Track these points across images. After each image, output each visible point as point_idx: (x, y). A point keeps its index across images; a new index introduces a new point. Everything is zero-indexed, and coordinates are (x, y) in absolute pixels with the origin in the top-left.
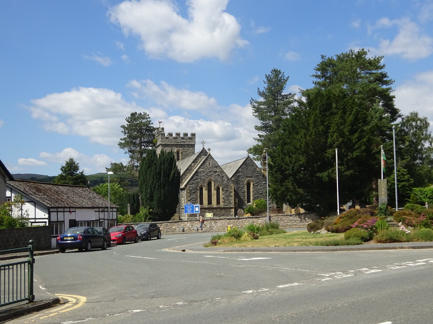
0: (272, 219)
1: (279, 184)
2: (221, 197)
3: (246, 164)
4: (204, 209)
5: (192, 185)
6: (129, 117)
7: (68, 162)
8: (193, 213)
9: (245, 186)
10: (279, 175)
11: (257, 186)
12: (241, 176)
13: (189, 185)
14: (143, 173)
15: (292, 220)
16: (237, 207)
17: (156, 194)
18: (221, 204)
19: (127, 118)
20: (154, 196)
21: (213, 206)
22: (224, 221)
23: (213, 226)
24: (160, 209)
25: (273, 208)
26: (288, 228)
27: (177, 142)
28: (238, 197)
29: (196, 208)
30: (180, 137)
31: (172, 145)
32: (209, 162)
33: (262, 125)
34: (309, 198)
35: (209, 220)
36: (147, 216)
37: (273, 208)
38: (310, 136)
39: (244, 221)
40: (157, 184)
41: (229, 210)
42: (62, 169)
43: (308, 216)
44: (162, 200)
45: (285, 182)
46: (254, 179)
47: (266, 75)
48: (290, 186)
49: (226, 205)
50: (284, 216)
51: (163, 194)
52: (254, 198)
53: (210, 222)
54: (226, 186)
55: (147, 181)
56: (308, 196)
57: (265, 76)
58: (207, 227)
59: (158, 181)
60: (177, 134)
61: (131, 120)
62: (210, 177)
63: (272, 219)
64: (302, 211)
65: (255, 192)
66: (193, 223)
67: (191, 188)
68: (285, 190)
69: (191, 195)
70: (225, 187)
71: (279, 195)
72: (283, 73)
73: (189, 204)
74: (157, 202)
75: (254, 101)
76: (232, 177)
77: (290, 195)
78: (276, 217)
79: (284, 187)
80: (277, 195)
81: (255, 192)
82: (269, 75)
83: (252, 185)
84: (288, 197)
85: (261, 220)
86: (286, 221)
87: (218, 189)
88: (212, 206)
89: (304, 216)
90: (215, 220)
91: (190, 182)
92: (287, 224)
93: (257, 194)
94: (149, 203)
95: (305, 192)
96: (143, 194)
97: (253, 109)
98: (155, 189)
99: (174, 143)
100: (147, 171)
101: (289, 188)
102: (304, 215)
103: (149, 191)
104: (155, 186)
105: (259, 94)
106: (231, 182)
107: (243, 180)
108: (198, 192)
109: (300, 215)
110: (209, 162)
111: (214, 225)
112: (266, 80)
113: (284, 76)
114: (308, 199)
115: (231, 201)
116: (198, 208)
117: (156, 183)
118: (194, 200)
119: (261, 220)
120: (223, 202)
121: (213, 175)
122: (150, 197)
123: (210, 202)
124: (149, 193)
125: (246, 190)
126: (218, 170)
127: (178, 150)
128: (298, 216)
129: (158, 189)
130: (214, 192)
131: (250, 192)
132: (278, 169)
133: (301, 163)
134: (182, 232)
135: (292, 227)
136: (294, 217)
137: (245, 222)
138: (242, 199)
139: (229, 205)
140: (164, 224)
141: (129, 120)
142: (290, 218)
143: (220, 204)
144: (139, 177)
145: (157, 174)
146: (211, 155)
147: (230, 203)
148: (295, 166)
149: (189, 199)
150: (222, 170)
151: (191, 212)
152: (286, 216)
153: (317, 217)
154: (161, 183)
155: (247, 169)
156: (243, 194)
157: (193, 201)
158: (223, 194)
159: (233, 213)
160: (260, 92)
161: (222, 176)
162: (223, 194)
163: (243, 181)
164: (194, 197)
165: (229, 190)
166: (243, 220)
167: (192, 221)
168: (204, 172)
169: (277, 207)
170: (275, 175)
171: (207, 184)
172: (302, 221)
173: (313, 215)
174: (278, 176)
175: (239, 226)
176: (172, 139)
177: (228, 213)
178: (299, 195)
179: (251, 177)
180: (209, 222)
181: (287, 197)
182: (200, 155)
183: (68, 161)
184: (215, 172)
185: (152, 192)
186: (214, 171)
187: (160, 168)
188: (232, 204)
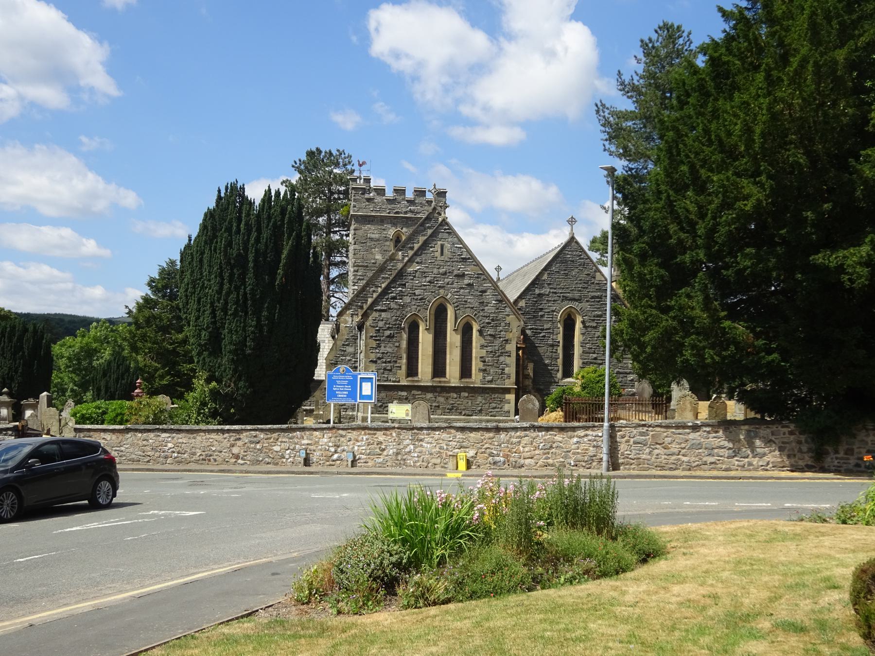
0: (623, 437)
1: (654, 304)
2: (474, 355)
4: (418, 391)
5: (384, 315)
6: (300, 161)
7: (164, 269)
8: (353, 402)
9: (559, 325)
10: (653, 270)
12: (548, 295)
14: (192, 258)
15: (699, 446)
16: (531, 387)
17: (230, 331)
18: (473, 375)
19: (296, 163)
20: (223, 336)
21: (449, 382)
22: (445, 435)
23: (407, 450)
24: (241, 384)
25: (641, 394)
26: (682, 477)
27: (397, 213)
28: (535, 358)
29: (364, 384)
30: (404, 199)
31: (382, 220)
32: (442, 246)
33: (624, 172)
34: (773, 361)
35: (394, 428)
36: (204, 404)
37: (641, 394)
38: (796, 80)
39: (515, 440)
40: (233, 296)
41: (500, 396)
42: (151, 283)
43: (764, 431)
44: (248, 351)
45: (675, 295)
46: (586, 306)
47: (642, 41)
48: (698, 312)
49: (491, 382)
50: (667, 427)
51: (253, 332)
52: (583, 363)
53: (399, 434)
54: (493, 320)
55: (203, 287)
56: (769, 352)
57: (640, 43)
58: (385, 453)
59: (237, 288)
60: (396, 191)
61: (306, 168)
62: (442, 291)
63: (623, 437)
64: (735, 410)
66: (342, 436)
67: (381, 324)
68: (675, 328)
69: (379, 346)
70: (490, 323)
71: (653, 347)
72: (690, 33)
73: (341, 370)
74: (231, 357)
75: (608, 109)
76: (520, 297)
77: (694, 347)
78: (635, 431)
79: (672, 314)
80: (642, 346)
82: (650, 40)
83: (578, 326)
84: (687, 353)
85: (580, 437)
86: (675, 447)
87: (466, 332)
88: (445, 382)
89: (749, 431)
90: (413, 429)
92: (679, 460)
93: (594, 353)
94: (207, 360)
95: (757, 336)
96: (191, 330)
97: (603, 129)
98: (226, 314)
99: (389, 213)
100: (202, 253)
101: (692, 319)
102: (746, 427)
103: (206, 319)
104: (226, 303)
105: (621, 90)
106: (508, 309)
107: (552, 308)
108: (401, 337)
109: (732, 428)
110: (442, 246)
111: (412, 447)
112: (642, 54)
113: (691, 43)
114: (769, 363)
115: (507, 369)
116: (369, 384)
117: (228, 294)
118: (390, 362)
119: (580, 437)
120: (480, 370)
122: (209, 340)
123: (439, 369)
124: (208, 327)
125: (560, 338)
126: (470, 270)
127: (399, 234)
128: (725, 430)
129: (235, 314)
130: (453, 339)
131: (573, 346)
132: (652, 245)
133: (745, 205)
134: (301, 468)
135: (698, 473)
136: (709, 432)
137: (519, 442)
138: (547, 365)
140: (247, 436)
141: (302, 167)
142: (692, 436)
143: (470, 376)
144: (182, 272)
145: (232, 261)
146: (447, 224)
147: (502, 374)
148: (718, 224)
149: (373, 357)
151: (348, 396)
152: (678, 427)
153: (803, 438)
154: (245, 294)
155: (567, 275)
157: (385, 362)
158: (482, 347)
159: (510, 407)
160: (622, 83)
162: (482, 347)
163: (553, 311)
164: (390, 350)
165: (502, 333)
166: (513, 434)
167: (339, 429)
168: (424, 274)
169: (655, 394)
170: (637, 268)
171: (433, 312)
172: (739, 450)
173: (786, 430)
174: (651, 272)
175: (498, 455)
176: (383, 204)
177: (494, 405)
178: (732, 348)
179: (579, 300)
180: (394, 434)
181: (682, 355)
182: (422, 228)
183: (165, 266)
184: (457, 276)
185: (218, 324)
186: (456, 272)
187: (246, 243)
188: (509, 377)
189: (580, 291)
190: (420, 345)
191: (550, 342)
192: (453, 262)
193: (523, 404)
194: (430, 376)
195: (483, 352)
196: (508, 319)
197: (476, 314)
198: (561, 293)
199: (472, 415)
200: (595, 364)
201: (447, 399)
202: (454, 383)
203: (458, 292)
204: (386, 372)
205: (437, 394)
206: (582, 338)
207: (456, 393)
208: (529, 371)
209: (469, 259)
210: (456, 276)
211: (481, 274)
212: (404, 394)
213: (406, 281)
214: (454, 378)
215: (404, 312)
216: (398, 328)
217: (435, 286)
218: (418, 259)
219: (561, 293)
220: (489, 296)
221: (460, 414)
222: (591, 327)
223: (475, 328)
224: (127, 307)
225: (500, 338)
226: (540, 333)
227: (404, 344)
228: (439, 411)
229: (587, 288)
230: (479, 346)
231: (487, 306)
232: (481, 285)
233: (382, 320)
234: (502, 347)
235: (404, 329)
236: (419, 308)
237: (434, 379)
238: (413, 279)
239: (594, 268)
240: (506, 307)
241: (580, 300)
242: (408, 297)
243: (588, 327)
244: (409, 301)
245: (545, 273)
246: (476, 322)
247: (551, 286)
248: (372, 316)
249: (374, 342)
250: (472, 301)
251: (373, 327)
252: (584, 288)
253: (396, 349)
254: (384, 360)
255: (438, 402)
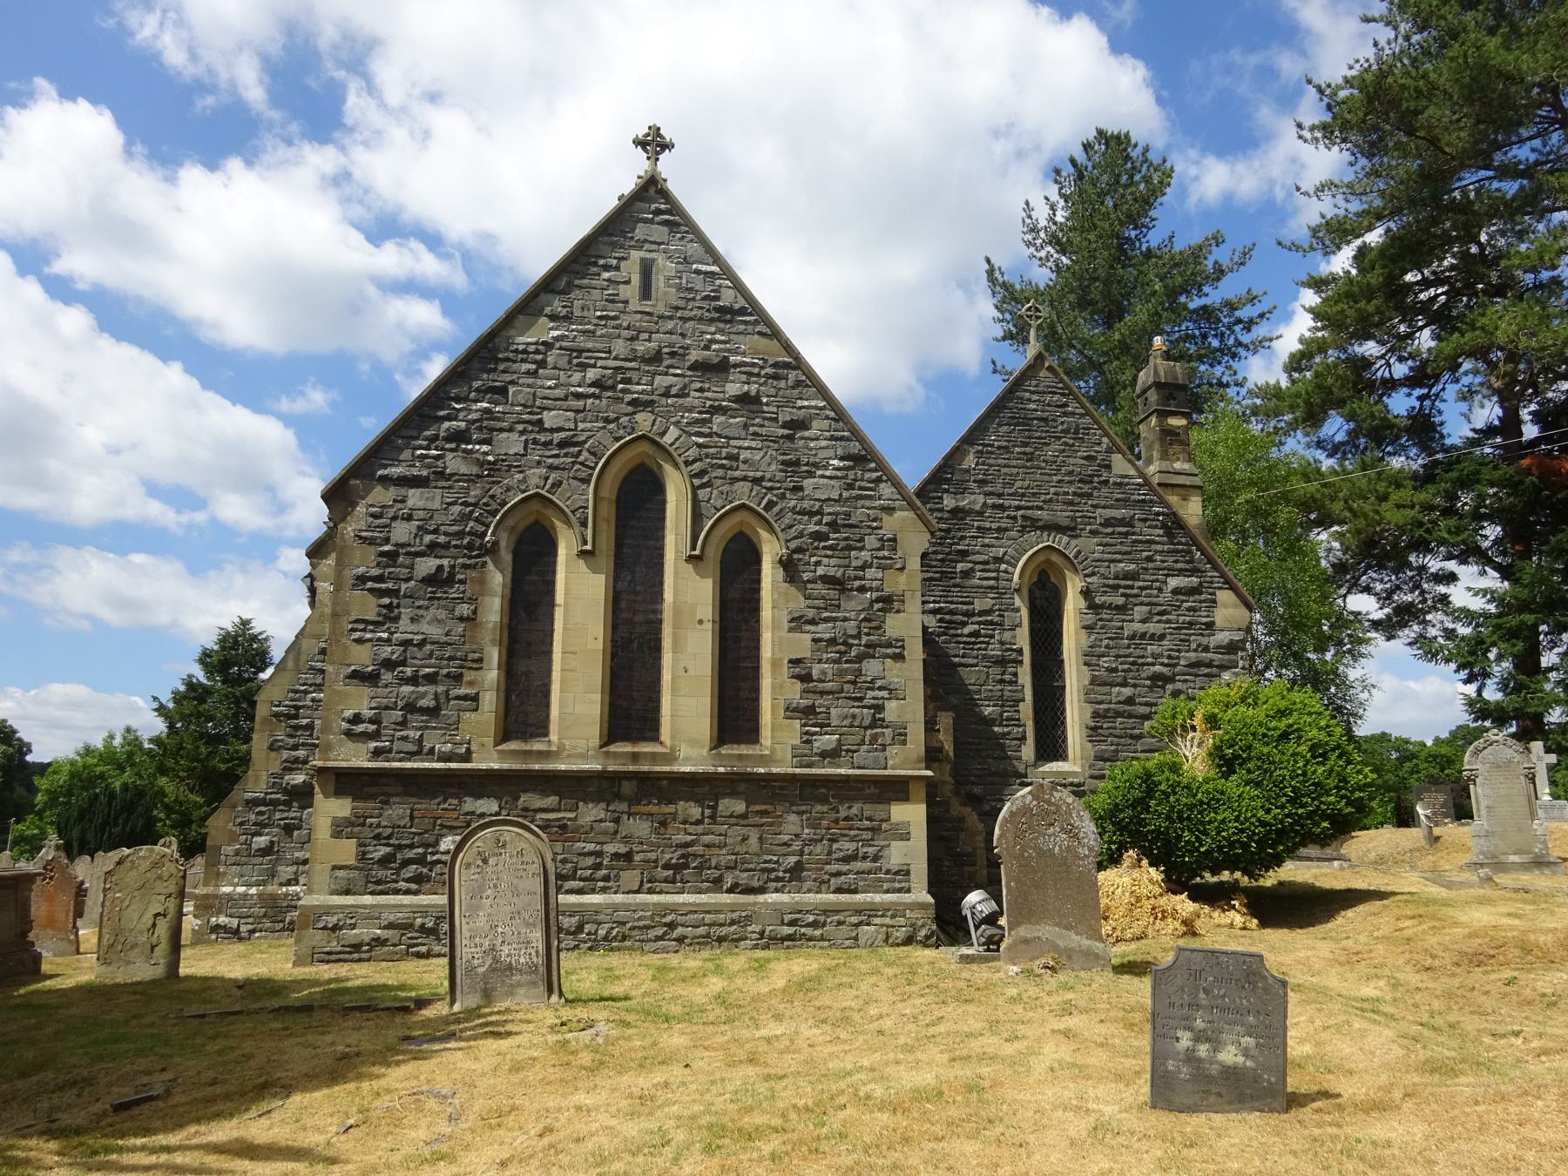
2: (766, 653)
3: (1024, 421)
4: (544, 793)
5: (415, 498)
7: (228, 633)
9: (1018, 602)
11: (1122, 609)
12: (980, 513)
13: (381, 496)
21: (670, 758)
28: (954, 700)
32: (647, 269)
41: (869, 810)
46: (1088, 544)
49: (831, 755)
52: (1096, 715)
54: (833, 525)
62: (644, 420)
65: (1105, 662)
67: (402, 532)
69: (389, 616)
70: (819, 536)
81: (1105, 662)
83: (1073, 604)
88: (654, 757)
91: (397, 461)
93: (1124, 684)
107: (994, 552)
108: (482, 582)
110: (647, 269)
115: (892, 706)
120: (792, 711)
121: (682, 394)
125: (1023, 638)
126: (746, 348)
131: (1060, 664)
138: (989, 722)
139: (862, 755)
147: (872, 726)
150: (788, 348)
156: (995, 671)
157: (414, 680)
161: (784, 416)
163: (999, 560)
164: (435, 632)
165: (870, 573)
168: (577, 357)
171: (610, 490)
177: (848, 846)
179: (1070, 530)
183: (230, 629)
184: (701, 367)
186: (694, 355)
188: (901, 737)
189: (1071, 503)
190: (559, 614)
191: (995, 651)
192: (684, 319)
193: (1019, 835)
194: (592, 732)
195: (802, 644)
196: (890, 524)
197: (770, 506)
198: (1018, 508)
199: (761, 890)
200: (1130, 716)
201: (663, 824)
202: (687, 760)
203: (703, 422)
204: (416, 720)
205: (624, 807)
206: (1085, 640)
207: (699, 801)
208: (941, 737)
209: (742, 311)
210: (695, 367)
211: (787, 366)
212: (488, 806)
213: (507, 377)
214: (693, 743)
215: (496, 490)
216: (470, 547)
217: (619, 400)
218: (557, 305)
219: (1018, 508)
220: (817, 441)
221: (717, 884)
222: (1110, 607)
223: (771, 551)
224: (155, 699)
225: (862, 589)
226: (964, 624)
227: (493, 610)
228: (631, 877)
229: (1090, 496)
230: (784, 617)
231: (811, 474)
232: (790, 402)
233: (409, 518)
234: (873, 621)
235: (493, 550)
236: (554, 476)
237: (612, 748)
238: (534, 374)
239: (1105, 440)
240: (878, 480)
241: (1074, 529)
242: (514, 436)
243: (1102, 606)
244: (519, 449)
245: (965, 453)
246: (772, 530)
247: (987, 489)
248: (370, 499)
249: (372, 601)
250: (758, 456)
251: (371, 542)
252: (1081, 495)
253: (460, 628)
254: (409, 671)
255: (627, 839)
